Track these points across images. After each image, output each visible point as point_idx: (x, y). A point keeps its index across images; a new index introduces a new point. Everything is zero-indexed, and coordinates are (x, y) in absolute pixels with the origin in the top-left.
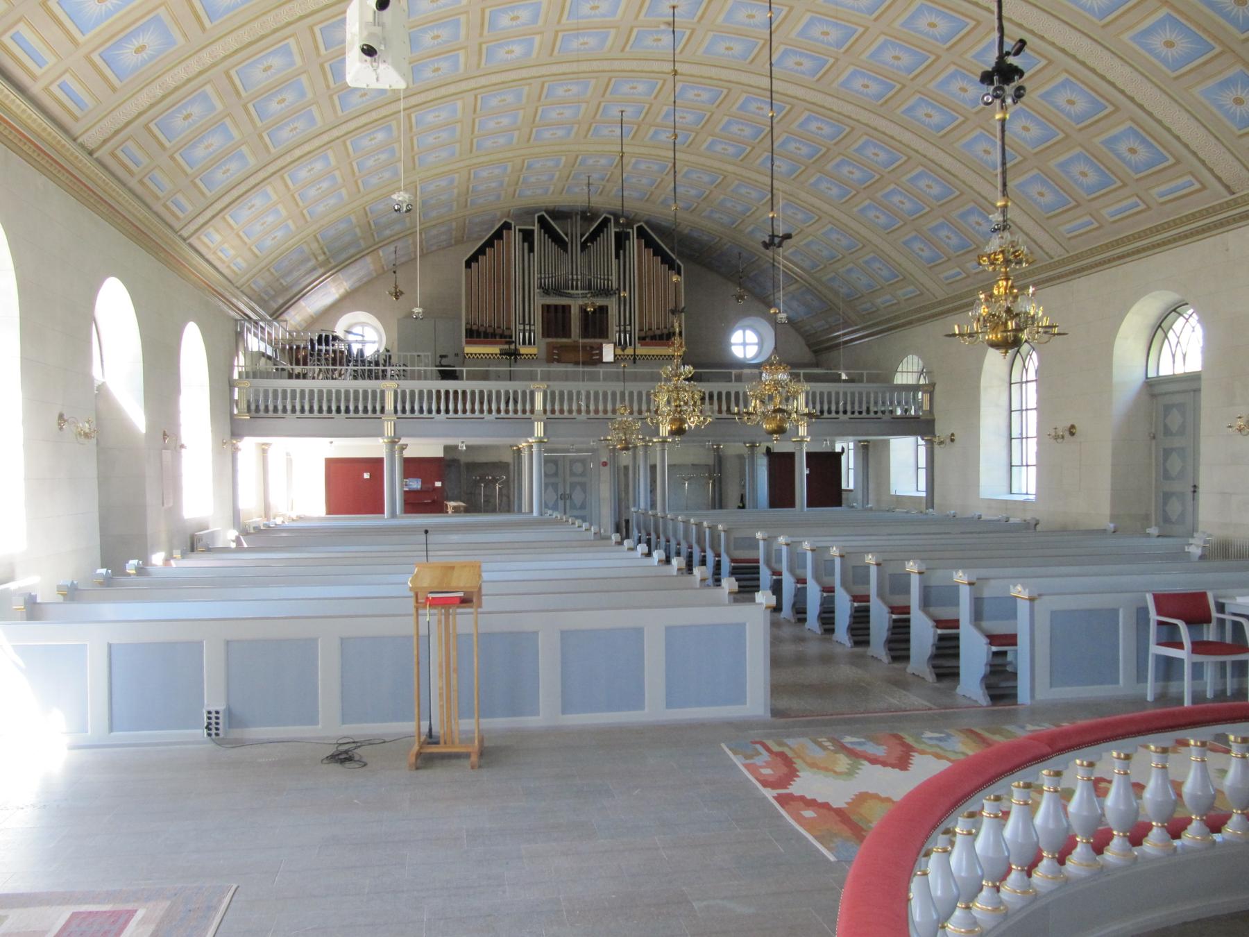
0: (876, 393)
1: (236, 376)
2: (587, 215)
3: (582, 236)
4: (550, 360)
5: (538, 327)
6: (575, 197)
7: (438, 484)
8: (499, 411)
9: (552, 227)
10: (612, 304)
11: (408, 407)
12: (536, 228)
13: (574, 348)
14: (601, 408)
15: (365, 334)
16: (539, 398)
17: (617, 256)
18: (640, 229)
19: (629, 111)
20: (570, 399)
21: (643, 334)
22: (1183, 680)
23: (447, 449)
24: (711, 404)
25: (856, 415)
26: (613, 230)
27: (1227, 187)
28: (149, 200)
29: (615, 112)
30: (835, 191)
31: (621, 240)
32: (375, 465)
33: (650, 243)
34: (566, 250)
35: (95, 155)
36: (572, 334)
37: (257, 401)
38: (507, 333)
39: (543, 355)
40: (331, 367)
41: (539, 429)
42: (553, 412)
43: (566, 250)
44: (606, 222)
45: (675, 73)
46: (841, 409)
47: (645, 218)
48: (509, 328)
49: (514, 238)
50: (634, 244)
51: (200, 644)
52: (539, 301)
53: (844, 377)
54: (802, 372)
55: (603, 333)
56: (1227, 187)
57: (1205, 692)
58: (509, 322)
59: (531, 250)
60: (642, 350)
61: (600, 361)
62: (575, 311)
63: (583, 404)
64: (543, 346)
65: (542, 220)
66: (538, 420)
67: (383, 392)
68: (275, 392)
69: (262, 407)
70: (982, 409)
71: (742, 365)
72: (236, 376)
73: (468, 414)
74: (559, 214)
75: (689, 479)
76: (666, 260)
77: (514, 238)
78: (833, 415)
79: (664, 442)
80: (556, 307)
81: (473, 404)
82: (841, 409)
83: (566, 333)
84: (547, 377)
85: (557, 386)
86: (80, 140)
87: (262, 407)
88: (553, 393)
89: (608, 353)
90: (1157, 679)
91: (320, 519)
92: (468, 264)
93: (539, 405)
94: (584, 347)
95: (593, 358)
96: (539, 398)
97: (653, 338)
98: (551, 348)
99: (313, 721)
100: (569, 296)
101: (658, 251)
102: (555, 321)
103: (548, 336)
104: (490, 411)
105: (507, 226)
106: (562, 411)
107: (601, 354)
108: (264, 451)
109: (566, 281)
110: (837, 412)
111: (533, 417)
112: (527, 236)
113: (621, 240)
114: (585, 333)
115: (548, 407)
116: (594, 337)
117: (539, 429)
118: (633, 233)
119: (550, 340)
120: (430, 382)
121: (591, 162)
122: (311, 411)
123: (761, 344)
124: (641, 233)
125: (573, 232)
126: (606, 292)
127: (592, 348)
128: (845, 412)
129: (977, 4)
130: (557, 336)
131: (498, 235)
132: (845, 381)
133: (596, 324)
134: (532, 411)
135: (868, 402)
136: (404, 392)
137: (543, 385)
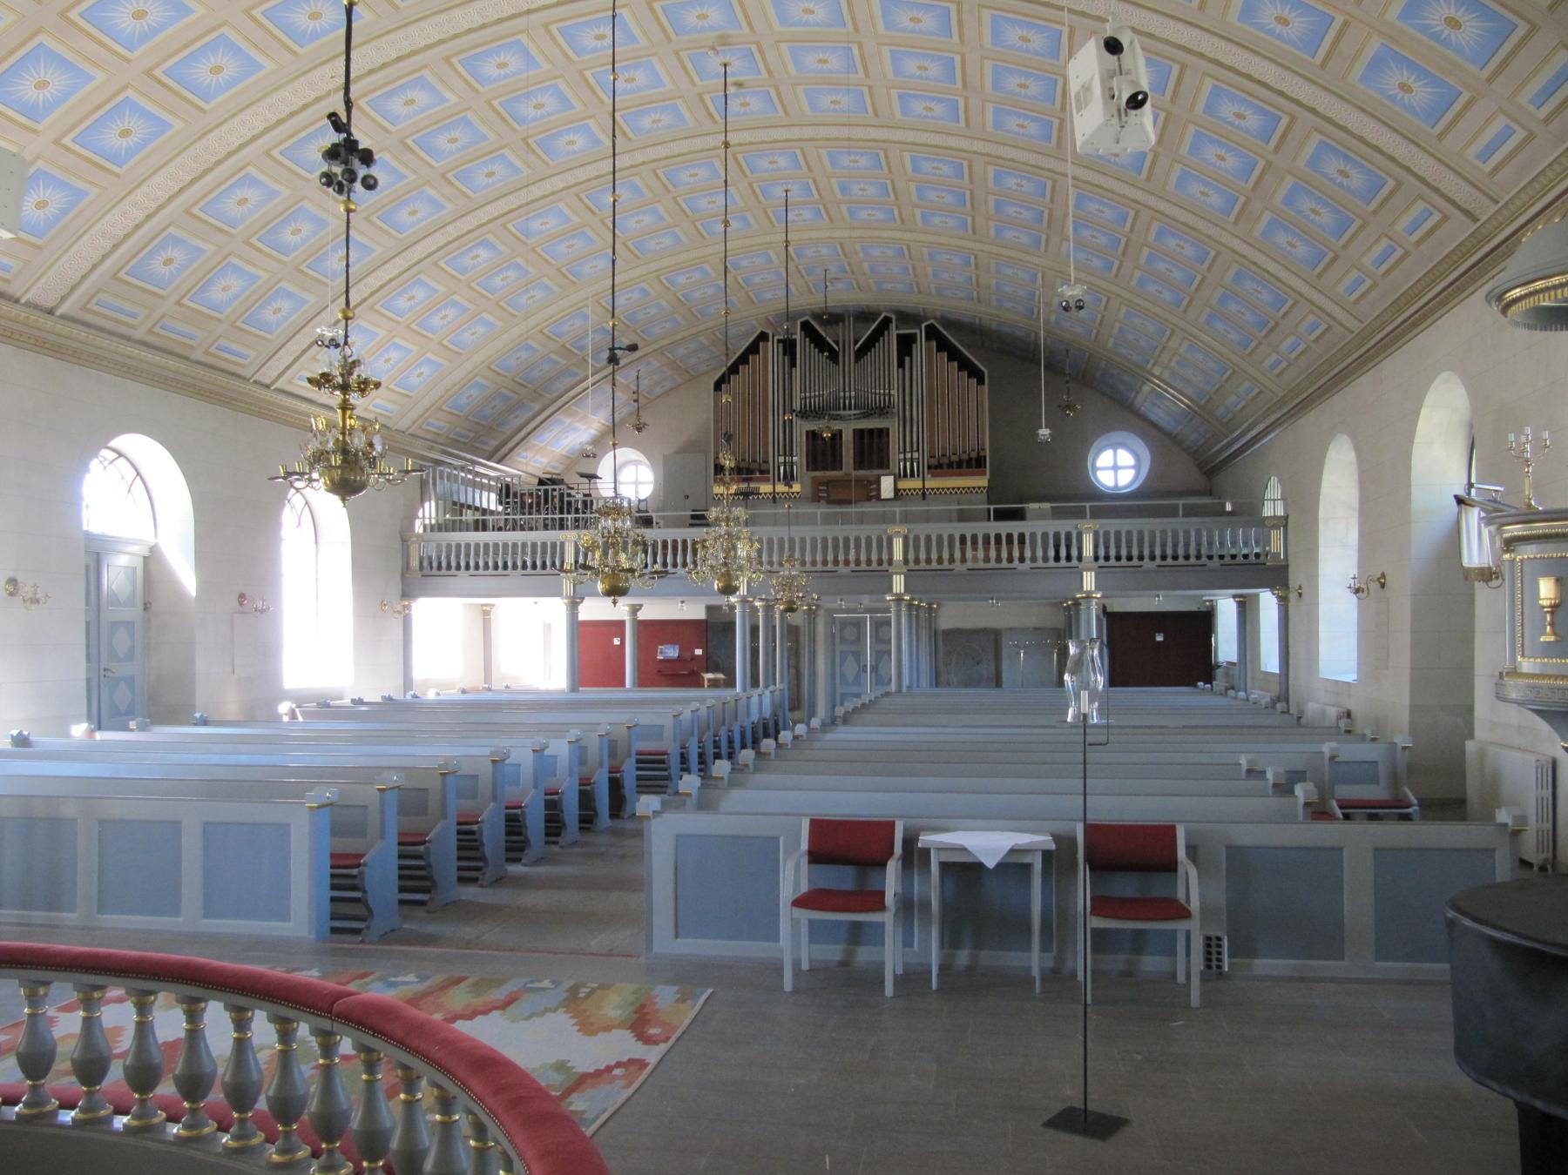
0: (1198, 533)
1: (419, 529)
2: (864, 316)
3: (856, 342)
4: (816, 499)
5: (800, 458)
6: (842, 296)
7: (699, 652)
8: (1034, 559)
9: (819, 334)
10: (893, 425)
11: (1063, 553)
12: (798, 336)
13: (845, 483)
14: (863, 557)
15: (631, 477)
16: (898, 545)
17: (901, 365)
18: (932, 333)
19: (795, 190)
20: (858, 547)
21: (934, 462)
22: (883, 945)
23: (710, 609)
24: (975, 549)
25: (1170, 561)
26: (894, 332)
27: (1467, 213)
28: (186, 353)
29: (779, 192)
30: (1302, 250)
31: (906, 344)
32: (618, 626)
33: (944, 345)
34: (836, 361)
35: (58, 313)
36: (843, 464)
37: (439, 558)
38: (763, 467)
39: (808, 492)
40: (557, 516)
41: (898, 583)
42: (917, 561)
43: (836, 361)
44: (887, 321)
45: (727, 145)
46: (1146, 553)
47: (938, 314)
48: (766, 462)
49: (771, 350)
50: (921, 348)
51: (776, 839)
52: (802, 428)
53: (1229, 507)
54: (1181, 502)
55: (883, 464)
56: (1467, 213)
57: (1029, 969)
58: (766, 453)
59: (793, 364)
60: (932, 483)
61: (878, 497)
62: (848, 437)
63: (852, 552)
64: (808, 482)
65: (806, 326)
66: (1088, 570)
67: (562, 544)
68: (449, 546)
69: (444, 565)
70: (1321, 550)
71: (1095, 494)
72: (419, 529)
73: (1063, 562)
74: (834, 318)
75: (1025, 647)
76: (965, 365)
77: (771, 350)
78: (1135, 562)
79: (899, 600)
80: (871, 431)
81: (685, 556)
82: (1146, 553)
83: (836, 463)
84: (906, 519)
85: (923, 529)
86: (23, 301)
87: (444, 565)
88: (917, 539)
89: (887, 485)
90: (942, 945)
91: (562, 692)
92: (718, 386)
93: (898, 554)
94: (859, 481)
95: (870, 492)
96: (898, 545)
97: (960, 464)
98: (817, 483)
99: (176, 912)
100: (841, 418)
101: (954, 355)
102: (823, 453)
103: (815, 469)
104: (1022, 559)
105: (763, 337)
106: (869, 562)
107: (879, 489)
108: (486, 613)
109: (837, 399)
110: (1141, 558)
111: (1081, 566)
112: (789, 347)
113: (906, 344)
114: (860, 463)
115: (911, 556)
116: (870, 468)
117: (898, 583)
118: (920, 333)
119: (819, 474)
120: (1041, 523)
121: (809, 252)
122: (544, 566)
123: (1137, 467)
124: (932, 333)
125: (847, 338)
126: (883, 411)
127: (870, 483)
128: (1153, 558)
129: (1048, 5)
130: (824, 469)
131: (753, 349)
132: (1230, 514)
133: (872, 449)
134: (1080, 558)
135: (1199, 545)
136: (1107, 534)
137: (903, 529)
